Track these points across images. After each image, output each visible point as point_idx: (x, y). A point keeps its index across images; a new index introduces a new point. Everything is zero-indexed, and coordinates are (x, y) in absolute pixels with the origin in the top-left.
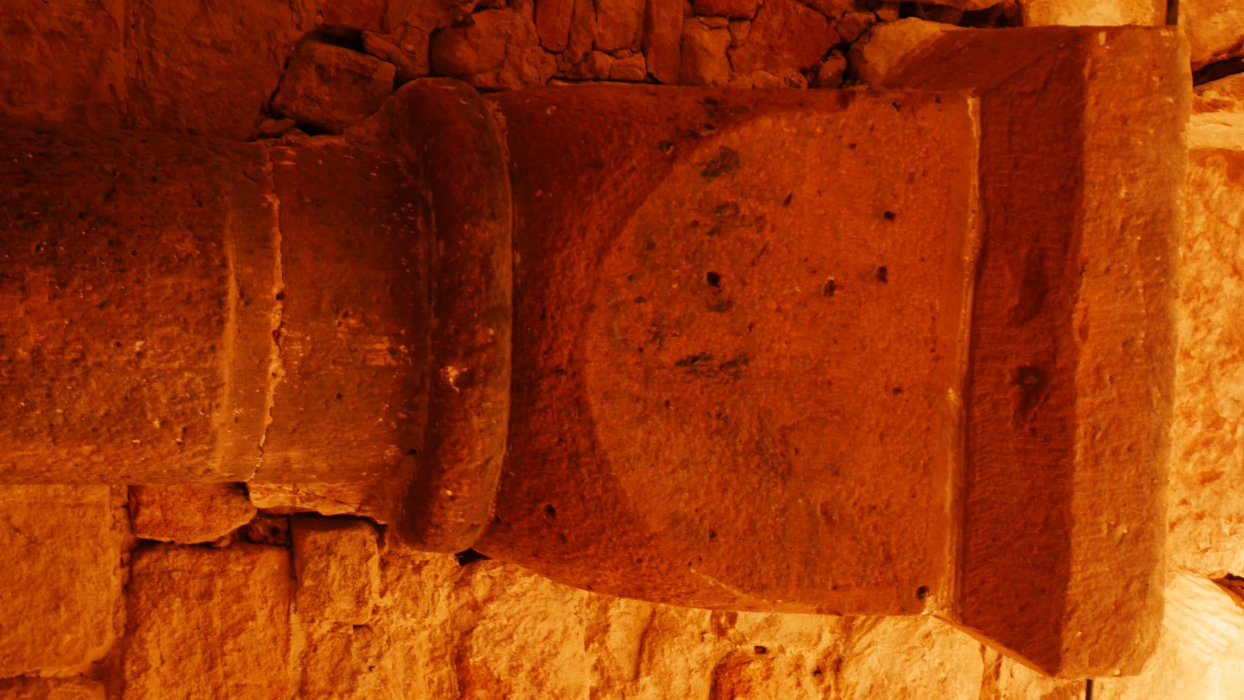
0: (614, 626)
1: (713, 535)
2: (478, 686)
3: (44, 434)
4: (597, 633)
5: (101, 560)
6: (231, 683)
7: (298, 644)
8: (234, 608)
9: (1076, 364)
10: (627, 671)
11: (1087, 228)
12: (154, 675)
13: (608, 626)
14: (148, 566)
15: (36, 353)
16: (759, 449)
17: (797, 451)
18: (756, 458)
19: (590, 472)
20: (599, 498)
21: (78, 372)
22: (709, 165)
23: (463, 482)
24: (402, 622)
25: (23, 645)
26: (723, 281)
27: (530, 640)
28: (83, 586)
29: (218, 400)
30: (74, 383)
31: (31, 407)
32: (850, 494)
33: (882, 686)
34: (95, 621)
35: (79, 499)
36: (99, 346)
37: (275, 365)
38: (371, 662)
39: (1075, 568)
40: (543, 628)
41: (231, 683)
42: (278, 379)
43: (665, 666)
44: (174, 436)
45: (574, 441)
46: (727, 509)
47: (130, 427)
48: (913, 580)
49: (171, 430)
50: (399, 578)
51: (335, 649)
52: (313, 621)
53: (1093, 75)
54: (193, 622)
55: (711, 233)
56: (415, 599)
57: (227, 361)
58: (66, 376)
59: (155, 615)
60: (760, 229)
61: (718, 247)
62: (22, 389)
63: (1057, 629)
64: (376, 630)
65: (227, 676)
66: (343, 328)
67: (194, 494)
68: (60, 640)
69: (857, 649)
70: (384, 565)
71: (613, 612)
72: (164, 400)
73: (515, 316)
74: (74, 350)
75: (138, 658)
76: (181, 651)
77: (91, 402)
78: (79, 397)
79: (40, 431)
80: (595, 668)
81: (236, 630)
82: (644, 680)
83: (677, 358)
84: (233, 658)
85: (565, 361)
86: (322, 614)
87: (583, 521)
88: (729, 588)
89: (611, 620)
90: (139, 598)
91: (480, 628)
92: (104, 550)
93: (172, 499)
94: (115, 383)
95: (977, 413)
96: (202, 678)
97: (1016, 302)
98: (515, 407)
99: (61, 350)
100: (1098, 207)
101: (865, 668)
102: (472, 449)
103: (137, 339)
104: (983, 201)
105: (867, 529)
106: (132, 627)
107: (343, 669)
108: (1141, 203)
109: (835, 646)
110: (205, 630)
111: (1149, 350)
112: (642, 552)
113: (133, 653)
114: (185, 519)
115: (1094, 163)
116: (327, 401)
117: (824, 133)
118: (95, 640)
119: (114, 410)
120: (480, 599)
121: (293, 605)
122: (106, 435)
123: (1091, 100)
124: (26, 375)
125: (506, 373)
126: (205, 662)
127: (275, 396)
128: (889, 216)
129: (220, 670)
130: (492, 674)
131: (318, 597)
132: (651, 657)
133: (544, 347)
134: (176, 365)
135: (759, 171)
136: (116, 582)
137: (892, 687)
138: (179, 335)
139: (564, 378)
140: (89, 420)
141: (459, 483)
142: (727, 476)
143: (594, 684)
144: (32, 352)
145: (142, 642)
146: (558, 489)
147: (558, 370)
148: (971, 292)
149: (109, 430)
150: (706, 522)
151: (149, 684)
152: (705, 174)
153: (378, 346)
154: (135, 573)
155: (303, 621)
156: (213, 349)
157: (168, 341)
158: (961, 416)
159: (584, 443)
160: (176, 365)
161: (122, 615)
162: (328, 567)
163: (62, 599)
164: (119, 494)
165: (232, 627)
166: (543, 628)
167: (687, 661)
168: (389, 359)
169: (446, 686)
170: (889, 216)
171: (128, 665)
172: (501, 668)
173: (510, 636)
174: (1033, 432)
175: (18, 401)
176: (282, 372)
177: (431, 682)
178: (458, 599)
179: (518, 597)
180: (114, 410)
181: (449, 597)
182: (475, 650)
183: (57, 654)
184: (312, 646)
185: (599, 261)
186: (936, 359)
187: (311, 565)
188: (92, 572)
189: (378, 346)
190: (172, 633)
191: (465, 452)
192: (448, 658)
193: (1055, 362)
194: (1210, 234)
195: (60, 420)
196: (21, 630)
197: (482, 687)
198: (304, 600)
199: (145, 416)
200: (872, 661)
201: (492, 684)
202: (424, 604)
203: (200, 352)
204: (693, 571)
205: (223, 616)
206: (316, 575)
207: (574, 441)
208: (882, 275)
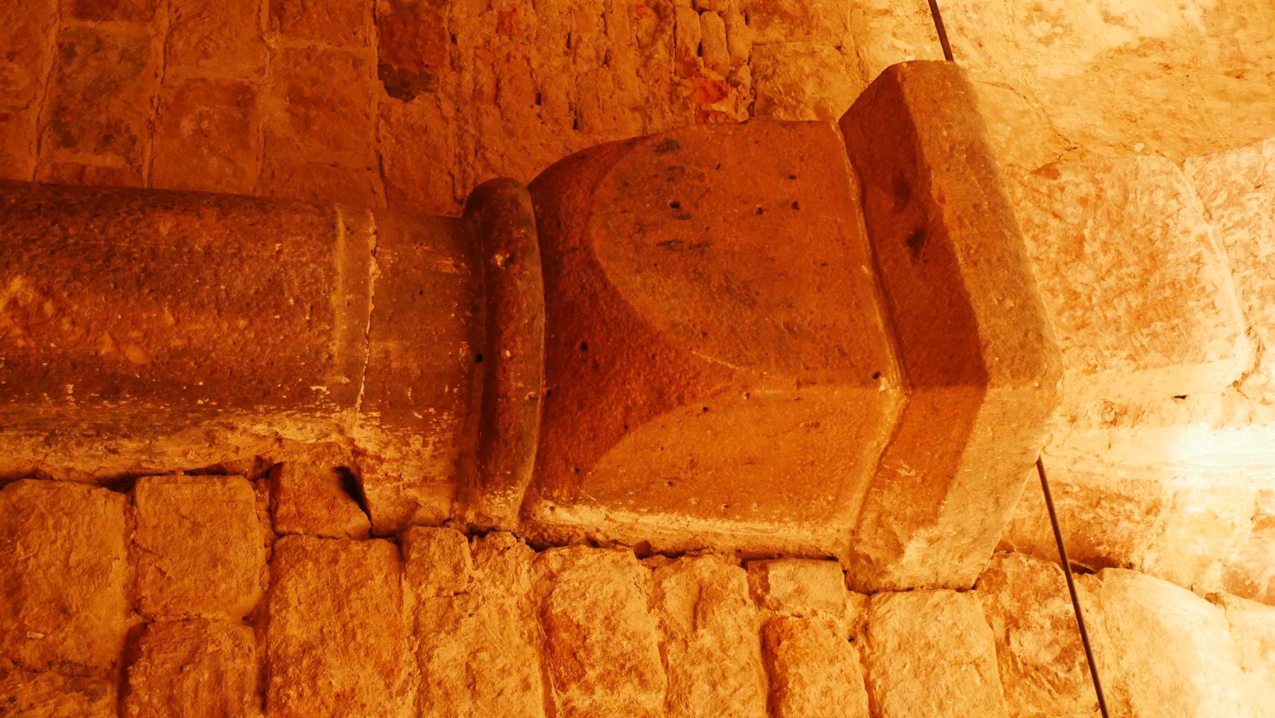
0: (668, 595)
1: (705, 334)
2: (562, 630)
3: (212, 306)
4: (656, 601)
5: (249, 536)
6: (356, 622)
7: (409, 600)
8: (356, 571)
9: (942, 216)
10: (686, 626)
11: (926, 150)
12: (294, 612)
13: (664, 594)
14: (286, 543)
15: (208, 250)
16: (728, 290)
17: (757, 293)
18: (728, 295)
19: (606, 303)
20: (616, 318)
21: (236, 261)
22: (658, 147)
23: (517, 339)
24: (493, 589)
25: (187, 591)
26: (682, 205)
27: (600, 597)
28: (236, 553)
29: (334, 284)
30: (233, 268)
31: (204, 282)
32: (804, 318)
33: (908, 642)
34: (245, 577)
35: (232, 497)
36: (251, 245)
37: (373, 268)
38: (470, 611)
39: (981, 321)
40: (609, 589)
41: (356, 622)
42: (376, 276)
43: (717, 622)
44: (304, 314)
45: (591, 286)
46: (712, 321)
47: (273, 303)
48: (867, 367)
49: (302, 306)
50: (487, 560)
51: (440, 605)
52: (420, 584)
53: (904, 79)
54: (323, 580)
55: (668, 180)
56: (502, 573)
57: (340, 257)
58: (227, 264)
59: (293, 572)
60: (702, 181)
61: (674, 188)
62: (197, 270)
63: (979, 357)
64: (472, 593)
65: (352, 616)
66: (419, 252)
67: (321, 494)
68: (217, 587)
69: (879, 614)
70: (474, 555)
71: (665, 584)
72: (296, 284)
73: (538, 227)
74: (233, 248)
75: (281, 600)
76: (314, 600)
77: (245, 282)
78: (236, 277)
79: (209, 303)
80: (659, 627)
81: (360, 585)
82: (701, 631)
83: (657, 242)
84: (357, 605)
85: (577, 243)
86: (427, 578)
87: (608, 340)
88: (724, 363)
89: (666, 590)
90: (279, 564)
91: (557, 590)
92: (252, 530)
93: (304, 497)
94: (262, 269)
95: (885, 269)
96: (333, 617)
97: (893, 205)
98: (546, 271)
99: (225, 246)
100: (930, 140)
101: (889, 627)
102: (519, 306)
103: (277, 242)
104: (856, 168)
105: (822, 337)
106: (275, 580)
107: (448, 618)
108: (960, 138)
109: (860, 616)
110: (334, 584)
111: (993, 211)
112: (653, 348)
113: (276, 597)
114: (314, 512)
115: (918, 119)
116: (413, 295)
117: (734, 135)
118: (245, 590)
119: (261, 290)
120: (554, 571)
121: (403, 575)
122: (255, 309)
123: (907, 91)
124: (200, 261)
125: (536, 255)
126: (334, 607)
127: (375, 287)
128: (793, 177)
129: (346, 611)
130: (572, 621)
131: (423, 565)
132: (704, 618)
133: (562, 239)
134: (304, 259)
135: (694, 151)
136: (262, 553)
137: (917, 642)
138: (306, 241)
139: (578, 252)
140: (244, 295)
141: (514, 341)
142: (708, 304)
143: (661, 639)
144: (204, 248)
145: (283, 589)
146: (586, 323)
147: (574, 249)
148: (861, 215)
149: (258, 305)
150: (698, 327)
151: (289, 616)
152: (656, 151)
153: (446, 262)
154: (277, 548)
155: (413, 585)
156: (330, 250)
157: (298, 245)
158: (875, 280)
159: (598, 286)
160: (304, 259)
161: (266, 575)
162: (429, 545)
163: (218, 560)
164: (263, 500)
165: (355, 584)
166: (609, 589)
167: (735, 619)
168: (454, 270)
169: (535, 634)
170: (793, 177)
171: (272, 605)
172: (579, 617)
173: (584, 595)
174: (926, 261)
175: (194, 277)
176: (379, 272)
177: (522, 633)
178: (536, 572)
179: (585, 568)
180: (261, 290)
181: (529, 571)
182: (555, 604)
183: (215, 597)
184: (420, 602)
185: (592, 192)
186: (848, 248)
187: (415, 544)
188: (243, 544)
189: (446, 262)
190: (308, 585)
191: (515, 310)
192: (534, 615)
193: (927, 219)
194: (1030, 198)
195: (223, 295)
196: (186, 581)
197: (565, 631)
198: (412, 569)
199: (284, 294)
200: (893, 622)
201: (573, 628)
202: (510, 574)
203: (321, 252)
204: (694, 353)
205: (347, 577)
206: (420, 551)
207: (591, 286)
208: (795, 206)
